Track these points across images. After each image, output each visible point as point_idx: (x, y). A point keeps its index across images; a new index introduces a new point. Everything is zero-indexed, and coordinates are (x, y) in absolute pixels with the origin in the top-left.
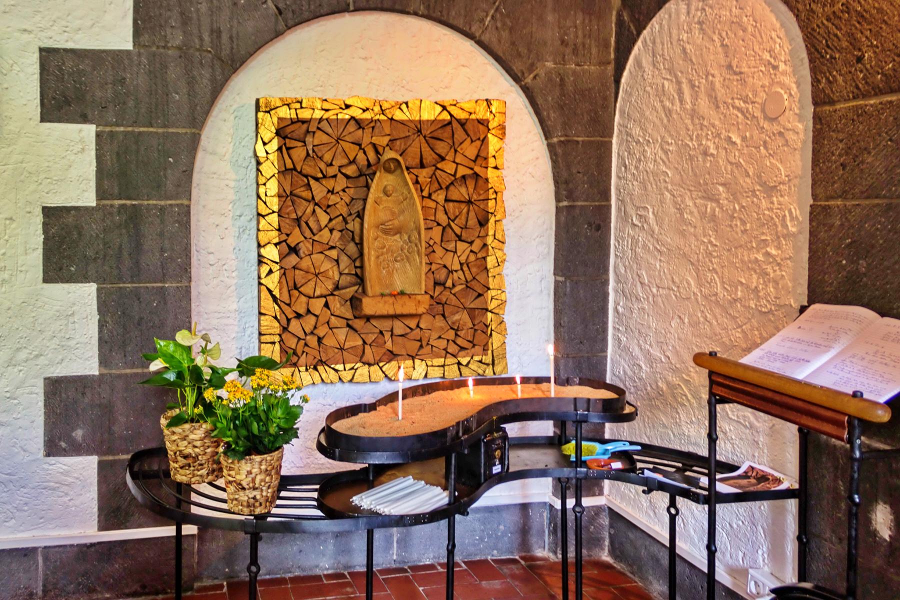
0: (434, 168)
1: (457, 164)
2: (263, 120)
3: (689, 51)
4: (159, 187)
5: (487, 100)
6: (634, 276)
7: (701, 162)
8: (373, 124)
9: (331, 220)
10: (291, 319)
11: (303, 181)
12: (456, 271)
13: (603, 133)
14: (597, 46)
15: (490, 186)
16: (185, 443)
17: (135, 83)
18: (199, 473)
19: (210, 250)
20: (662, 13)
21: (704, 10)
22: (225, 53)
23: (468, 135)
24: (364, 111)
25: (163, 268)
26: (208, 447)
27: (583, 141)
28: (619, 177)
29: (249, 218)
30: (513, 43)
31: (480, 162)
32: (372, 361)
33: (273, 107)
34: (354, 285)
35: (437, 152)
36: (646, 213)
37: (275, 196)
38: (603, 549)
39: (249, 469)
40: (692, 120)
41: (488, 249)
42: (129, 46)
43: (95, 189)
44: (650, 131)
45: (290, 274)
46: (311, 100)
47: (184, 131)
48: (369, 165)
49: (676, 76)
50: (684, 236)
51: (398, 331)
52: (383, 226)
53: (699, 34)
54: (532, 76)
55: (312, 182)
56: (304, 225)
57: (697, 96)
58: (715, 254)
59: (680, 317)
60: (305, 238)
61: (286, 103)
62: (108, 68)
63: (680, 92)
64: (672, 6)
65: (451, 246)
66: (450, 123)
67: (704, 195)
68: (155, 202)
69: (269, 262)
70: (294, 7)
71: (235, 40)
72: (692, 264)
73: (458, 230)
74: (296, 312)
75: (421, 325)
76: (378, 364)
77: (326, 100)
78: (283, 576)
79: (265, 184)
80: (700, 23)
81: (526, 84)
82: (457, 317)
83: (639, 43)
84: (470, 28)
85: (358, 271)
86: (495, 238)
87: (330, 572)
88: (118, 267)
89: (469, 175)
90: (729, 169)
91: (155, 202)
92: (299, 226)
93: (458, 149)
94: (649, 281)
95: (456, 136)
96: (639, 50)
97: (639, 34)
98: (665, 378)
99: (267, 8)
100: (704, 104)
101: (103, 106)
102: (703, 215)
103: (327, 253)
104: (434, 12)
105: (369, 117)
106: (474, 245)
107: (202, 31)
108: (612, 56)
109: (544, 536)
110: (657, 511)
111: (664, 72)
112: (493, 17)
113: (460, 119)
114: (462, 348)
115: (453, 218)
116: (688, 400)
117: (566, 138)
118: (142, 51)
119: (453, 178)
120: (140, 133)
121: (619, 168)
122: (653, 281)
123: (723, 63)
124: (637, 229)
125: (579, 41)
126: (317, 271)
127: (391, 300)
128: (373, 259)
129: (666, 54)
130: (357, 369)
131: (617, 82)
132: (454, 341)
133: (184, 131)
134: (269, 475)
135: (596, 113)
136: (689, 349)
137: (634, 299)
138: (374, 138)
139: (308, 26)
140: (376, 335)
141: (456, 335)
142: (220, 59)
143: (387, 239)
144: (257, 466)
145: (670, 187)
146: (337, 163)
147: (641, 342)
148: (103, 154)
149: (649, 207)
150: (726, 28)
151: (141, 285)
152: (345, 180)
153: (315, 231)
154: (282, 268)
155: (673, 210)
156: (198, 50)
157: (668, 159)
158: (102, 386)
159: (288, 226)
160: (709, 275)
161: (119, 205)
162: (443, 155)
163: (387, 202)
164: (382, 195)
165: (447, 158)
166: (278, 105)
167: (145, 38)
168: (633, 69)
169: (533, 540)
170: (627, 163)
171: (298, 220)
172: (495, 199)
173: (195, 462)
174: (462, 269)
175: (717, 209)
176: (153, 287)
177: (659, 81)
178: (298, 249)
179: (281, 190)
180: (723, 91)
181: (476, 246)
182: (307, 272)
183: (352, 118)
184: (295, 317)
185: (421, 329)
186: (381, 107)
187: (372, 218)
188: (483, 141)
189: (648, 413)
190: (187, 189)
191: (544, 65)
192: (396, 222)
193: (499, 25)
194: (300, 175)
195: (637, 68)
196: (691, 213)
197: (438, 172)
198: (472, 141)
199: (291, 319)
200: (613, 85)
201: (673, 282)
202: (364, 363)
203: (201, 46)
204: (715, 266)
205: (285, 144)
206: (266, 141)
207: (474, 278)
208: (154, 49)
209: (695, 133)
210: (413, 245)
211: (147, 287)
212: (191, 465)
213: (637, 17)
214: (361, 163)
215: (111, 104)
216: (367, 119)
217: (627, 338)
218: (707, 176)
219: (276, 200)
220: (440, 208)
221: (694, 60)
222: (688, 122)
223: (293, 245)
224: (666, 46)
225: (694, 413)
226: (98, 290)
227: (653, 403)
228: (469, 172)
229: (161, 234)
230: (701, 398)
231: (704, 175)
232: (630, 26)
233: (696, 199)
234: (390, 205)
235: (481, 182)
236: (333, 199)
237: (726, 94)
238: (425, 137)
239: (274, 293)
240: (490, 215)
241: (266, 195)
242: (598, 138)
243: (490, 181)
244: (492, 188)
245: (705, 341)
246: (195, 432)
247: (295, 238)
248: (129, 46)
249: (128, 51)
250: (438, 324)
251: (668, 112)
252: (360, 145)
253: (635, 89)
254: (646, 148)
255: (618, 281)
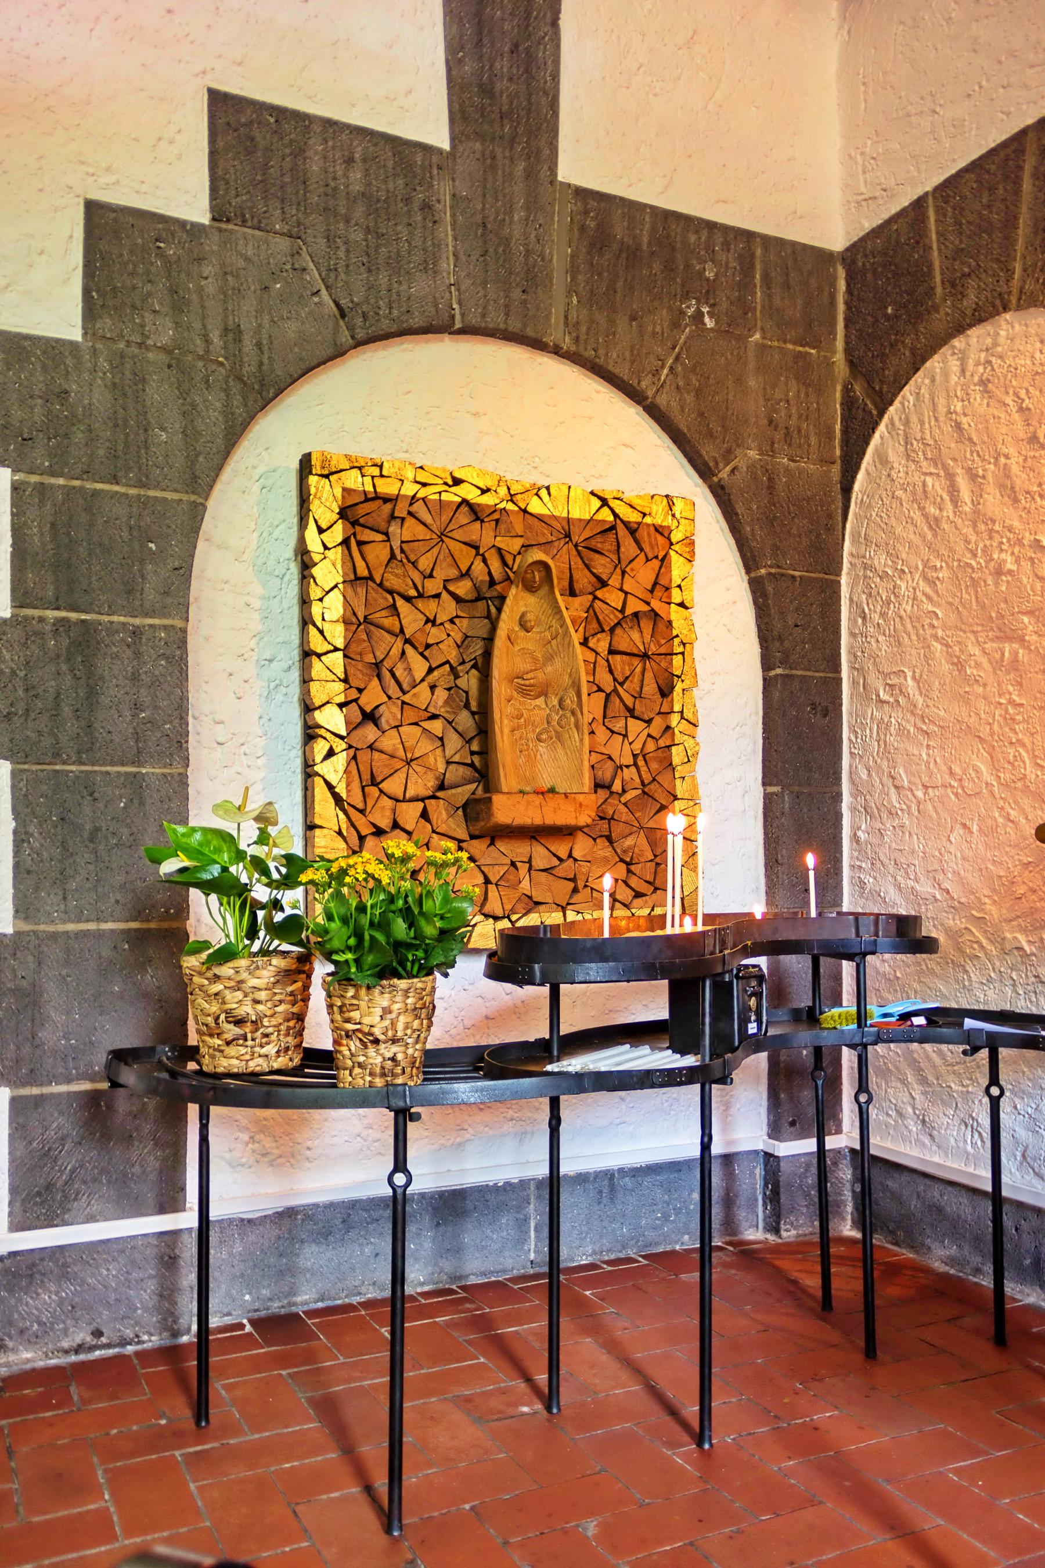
0: (591, 597)
1: (626, 593)
2: (317, 489)
3: (966, 427)
4: (130, 592)
5: (667, 496)
6: (885, 779)
7: (992, 588)
8: (496, 516)
9: (430, 670)
10: (366, 836)
11: (386, 599)
12: (627, 767)
13: (828, 568)
14: (818, 435)
15: (675, 633)
16: (239, 995)
17: (86, 402)
18: (263, 1051)
19: (217, 718)
20: (919, 377)
21: (989, 362)
22: (248, 369)
23: (641, 549)
24: (484, 492)
25: (137, 741)
26: (281, 1002)
27: (801, 577)
28: (852, 635)
29: (285, 665)
30: (701, 414)
31: (660, 594)
32: (499, 913)
33: (334, 470)
34: (470, 782)
35: (595, 571)
36: (902, 680)
37: (338, 621)
38: (844, 1219)
39: (385, 1004)
40: (975, 526)
41: (673, 734)
42: (76, 335)
43: (9, 586)
44: (904, 556)
45: (364, 757)
46: (397, 464)
47: (175, 496)
48: (492, 582)
49: (945, 467)
50: (967, 702)
51: (539, 863)
52: (520, 681)
53: (982, 398)
54: (728, 468)
55: (400, 603)
56: (387, 675)
57: (982, 490)
58: (1019, 718)
59: (964, 826)
60: (390, 698)
61: (356, 464)
62: (35, 369)
63: (953, 491)
64: (936, 364)
65: (619, 726)
66: (613, 528)
67: (998, 634)
68: (122, 619)
69: (328, 735)
70: (365, 308)
71: (265, 348)
72: (982, 740)
73: (629, 701)
74: (374, 825)
75: (576, 854)
76: (508, 917)
77: (421, 468)
78: (347, 1301)
79: (321, 600)
80: (983, 382)
81: (719, 481)
82: (629, 842)
83: (882, 428)
84: (639, 383)
85: (476, 760)
86: (682, 718)
87: (426, 1288)
88: (51, 733)
89: (644, 612)
90: (1039, 588)
91: (122, 619)
92: (379, 676)
93: (628, 569)
94: (910, 782)
95: (622, 549)
96: (882, 438)
97: (881, 414)
98: (942, 925)
99: (320, 304)
100: (993, 501)
101: (25, 436)
102: (998, 665)
103: (426, 724)
104: (586, 349)
105: (491, 502)
106: (654, 724)
107: (209, 327)
108: (838, 452)
109: (756, 1206)
110: (935, 1133)
111: (924, 464)
112: (671, 368)
113: (629, 522)
114: (638, 895)
115: (621, 680)
116: (982, 947)
117: (778, 570)
118: (99, 346)
119: (620, 616)
120: (96, 493)
121: (852, 621)
122: (918, 781)
123: (1022, 435)
124: (886, 707)
125: (793, 422)
126: (409, 756)
127: (538, 800)
128: (506, 731)
129: (928, 436)
130: (475, 925)
131: (847, 490)
132: (625, 882)
133: (175, 496)
134: (417, 1017)
135: (818, 536)
136: (981, 870)
137: (885, 816)
138: (498, 539)
139: (383, 349)
140: (506, 868)
141: (629, 871)
142: (239, 378)
143: (524, 704)
144: (399, 998)
145: (940, 633)
146: (440, 574)
147: (899, 878)
148: (25, 523)
149: (906, 670)
150: (1026, 384)
151: (96, 768)
152: (453, 604)
153: (405, 686)
154: (350, 747)
155: (946, 667)
156: (201, 358)
157: (937, 592)
158: (19, 955)
159: (360, 676)
160: (1011, 751)
161: (56, 618)
162: (604, 577)
163: (528, 642)
164: (517, 629)
165: (610, 582)
166: (342, 467)
167: (105, 324)
168: (872, 469)
169: (741, 1214)
170: (867, 610)
171: (377, 665)
172: (683, 653)
173: (257, 1030)
174: (635, 764)
175: (1021, 651)
176: (118, 772)
177: (917, 478)
178: (377, 716)
179: (349, 613)
180: (1024, 476)
181: (656, 728)
182: (393, 757)
183: (465, 501)
184: (373, 834)
185: (576, 860)
186: (509, 489)
187: (505, 663)
188: (663, 560)
189: (915, 985)
190: (181, 600)
191: (746, 455)
192: (540, 675)
193: (681, 383)
194: (379, 589)
195: (879, 466)
196: (978, 665)
197: (598, 604)
198: (648, 560)
199: (366, 836)
200: (840, 496)
201: (951, 773)
202: (487, 916)
203: (207, 351)
204: (1020, 736)
205: (354, 534)
206: (324, 526)
207: (654, 779)
208: (122, 345)
209: (981, 545)
210: (569, 714)
211: (108, 773)
212: (249, 1036)
213: (877, 388)
214: (480, 578)
215: (41, 435)
216: (488, 506)
217: (875, 878)
218: (1003, 605)
219: (340, 628)
220: (601, 662)
221: (975, 439)
222: (968, 531)
223: (368, 709)
224: (927, 426)
225: (993, 965)
226: (14, 774)
227: (924, 967)
228: (645, 608)
229: (135, 678)
230: (1004, 939)
231: (998, 604)
232: (866, 404)
233: (985, 643)
234: (530, 646)
235: (661, 626)
236: (435, 634)
237: (1030, 480)
238: (576, 546)
239: (337, 790)
240: (676, 679)
241: (323, 619)
242: (822, 575)
243: (674, 624)
244: (677, 636)
245: (1007, 853)
246: (258, 973)
247: (373, 697)
248: (76, 335)
249: (73, 344)
250: (600, 852)
251: (934, 524)
252: (476, 548)
253: (877, 497)
254: (898, 582)
255: (856, 793)
